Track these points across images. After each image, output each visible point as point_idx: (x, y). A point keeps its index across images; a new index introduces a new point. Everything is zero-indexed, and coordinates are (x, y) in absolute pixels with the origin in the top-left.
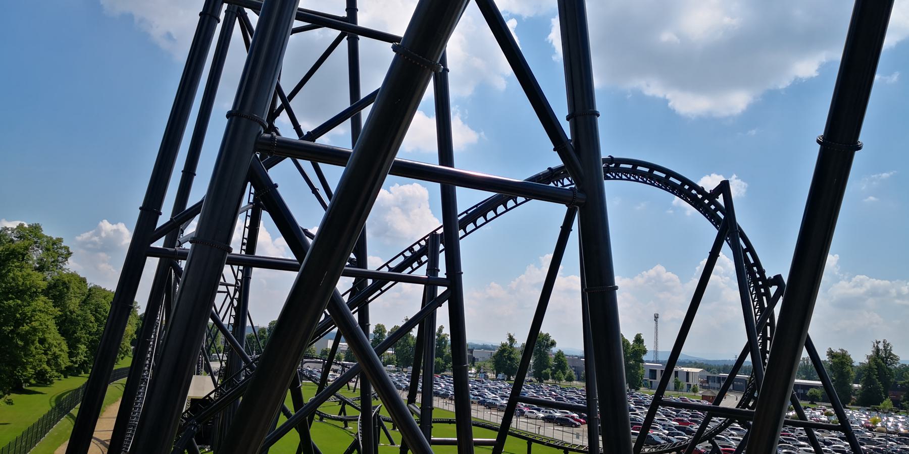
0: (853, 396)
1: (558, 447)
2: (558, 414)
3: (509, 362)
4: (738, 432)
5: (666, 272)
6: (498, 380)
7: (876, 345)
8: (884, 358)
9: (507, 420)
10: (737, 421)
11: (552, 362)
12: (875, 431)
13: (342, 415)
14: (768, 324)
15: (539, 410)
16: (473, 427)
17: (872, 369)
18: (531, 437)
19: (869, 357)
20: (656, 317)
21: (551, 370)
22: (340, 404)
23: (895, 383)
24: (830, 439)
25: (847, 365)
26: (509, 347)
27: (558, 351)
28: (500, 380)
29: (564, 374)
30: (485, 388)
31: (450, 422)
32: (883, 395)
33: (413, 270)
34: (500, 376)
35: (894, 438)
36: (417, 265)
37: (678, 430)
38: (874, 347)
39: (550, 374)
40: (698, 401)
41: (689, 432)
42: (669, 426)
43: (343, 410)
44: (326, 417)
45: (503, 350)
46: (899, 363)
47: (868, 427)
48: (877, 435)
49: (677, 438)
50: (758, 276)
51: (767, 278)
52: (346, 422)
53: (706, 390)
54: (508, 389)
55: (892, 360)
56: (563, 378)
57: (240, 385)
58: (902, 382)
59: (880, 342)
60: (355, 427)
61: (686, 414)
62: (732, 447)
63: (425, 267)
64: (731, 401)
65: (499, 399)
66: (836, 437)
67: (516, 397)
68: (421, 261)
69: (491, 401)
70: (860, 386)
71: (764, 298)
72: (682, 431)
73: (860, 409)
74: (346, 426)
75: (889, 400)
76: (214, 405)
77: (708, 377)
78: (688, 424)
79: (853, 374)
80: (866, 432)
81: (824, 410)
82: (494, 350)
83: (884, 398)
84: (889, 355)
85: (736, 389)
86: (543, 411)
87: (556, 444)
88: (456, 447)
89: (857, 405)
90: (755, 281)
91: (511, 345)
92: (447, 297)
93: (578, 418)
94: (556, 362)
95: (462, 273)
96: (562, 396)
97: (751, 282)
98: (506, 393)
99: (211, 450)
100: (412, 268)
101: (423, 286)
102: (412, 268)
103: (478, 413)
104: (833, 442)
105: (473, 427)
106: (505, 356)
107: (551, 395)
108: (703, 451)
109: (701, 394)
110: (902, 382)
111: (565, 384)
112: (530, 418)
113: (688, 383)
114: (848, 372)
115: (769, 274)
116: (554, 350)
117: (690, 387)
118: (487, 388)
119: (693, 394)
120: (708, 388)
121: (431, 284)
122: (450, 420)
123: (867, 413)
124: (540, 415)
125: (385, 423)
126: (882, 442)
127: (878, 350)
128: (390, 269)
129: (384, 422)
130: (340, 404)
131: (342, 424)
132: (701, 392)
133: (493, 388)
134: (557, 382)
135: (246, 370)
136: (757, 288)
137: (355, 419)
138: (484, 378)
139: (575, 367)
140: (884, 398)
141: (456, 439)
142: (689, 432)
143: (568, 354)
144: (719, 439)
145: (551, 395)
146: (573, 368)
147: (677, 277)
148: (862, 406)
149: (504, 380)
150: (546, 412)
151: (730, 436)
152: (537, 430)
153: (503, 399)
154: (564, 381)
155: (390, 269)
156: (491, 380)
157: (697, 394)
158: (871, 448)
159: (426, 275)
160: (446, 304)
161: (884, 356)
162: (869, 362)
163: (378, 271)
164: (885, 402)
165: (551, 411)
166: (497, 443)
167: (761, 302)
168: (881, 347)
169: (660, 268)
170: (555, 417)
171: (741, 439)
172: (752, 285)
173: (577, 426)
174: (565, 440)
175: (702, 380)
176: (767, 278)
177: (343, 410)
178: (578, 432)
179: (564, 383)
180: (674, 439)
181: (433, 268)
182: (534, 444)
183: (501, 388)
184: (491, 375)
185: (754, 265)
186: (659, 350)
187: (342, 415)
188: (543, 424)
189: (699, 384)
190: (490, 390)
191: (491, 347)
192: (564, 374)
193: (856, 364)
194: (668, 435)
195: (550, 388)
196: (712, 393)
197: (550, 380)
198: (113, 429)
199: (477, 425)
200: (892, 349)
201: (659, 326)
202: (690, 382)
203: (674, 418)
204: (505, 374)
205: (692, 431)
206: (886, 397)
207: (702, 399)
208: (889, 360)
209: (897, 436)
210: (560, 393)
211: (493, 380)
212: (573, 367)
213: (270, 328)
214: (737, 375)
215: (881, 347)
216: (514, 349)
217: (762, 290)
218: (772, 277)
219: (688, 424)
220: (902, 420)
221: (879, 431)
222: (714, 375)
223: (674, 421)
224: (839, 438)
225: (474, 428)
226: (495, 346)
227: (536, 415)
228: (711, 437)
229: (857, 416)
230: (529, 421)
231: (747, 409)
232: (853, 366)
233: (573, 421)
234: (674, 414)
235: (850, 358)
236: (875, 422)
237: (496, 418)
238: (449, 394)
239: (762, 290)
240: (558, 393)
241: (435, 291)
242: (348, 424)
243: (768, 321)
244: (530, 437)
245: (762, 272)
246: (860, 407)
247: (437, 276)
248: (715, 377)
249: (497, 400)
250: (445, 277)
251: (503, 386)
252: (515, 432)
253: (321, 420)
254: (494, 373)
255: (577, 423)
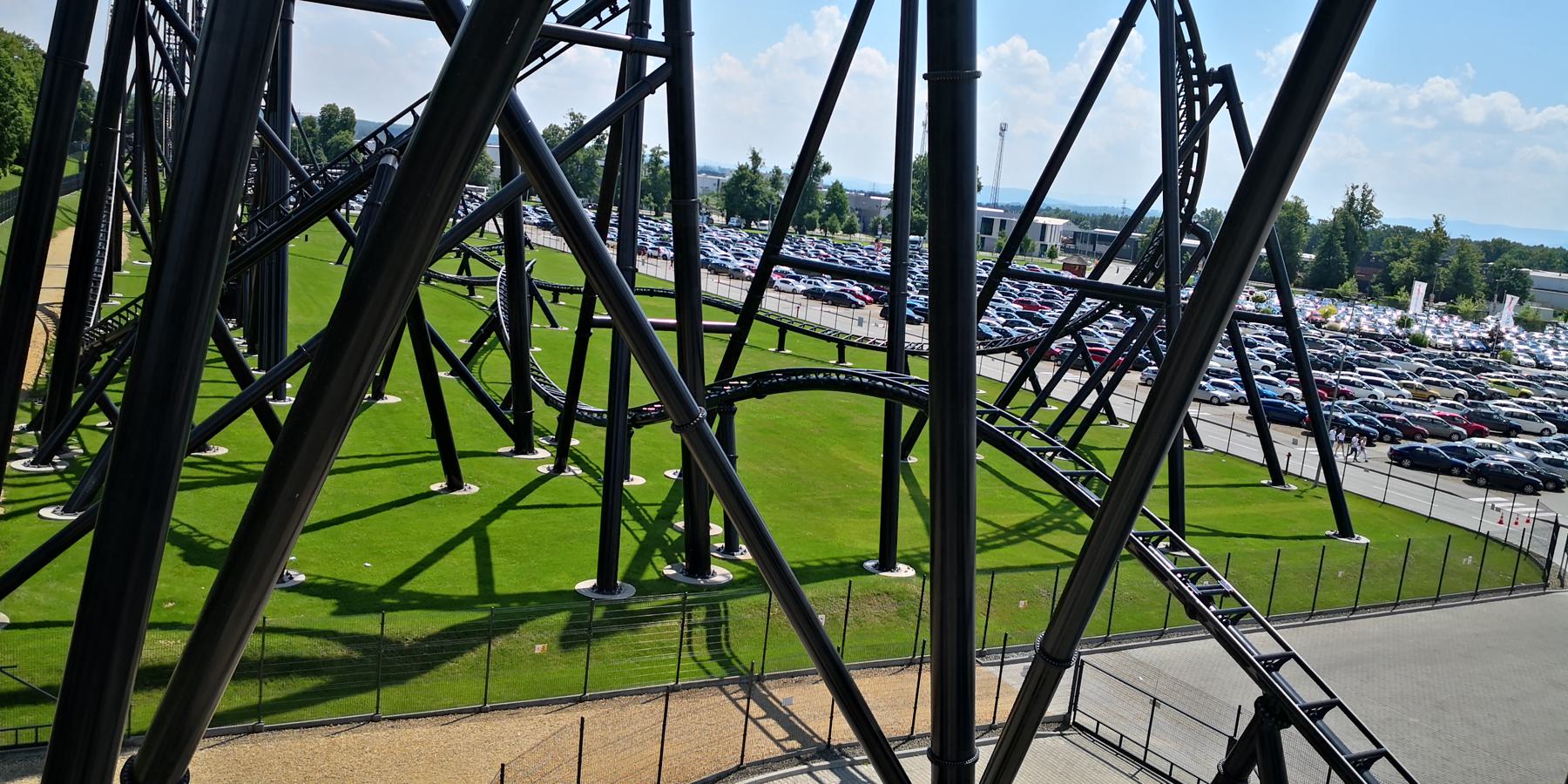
0: (1300, 272)
1: (829, 339)
2: (828, 286)
3: (749, 198)
4: (1115, 323)
5: (1028, 50)
6: (730, 227)
7: (1350, 193)
8: (1359, 213)
9: (755, 295)
10: (1121, 306)
11: (823, 201)
12: (1325, 328)
13: (464, 276)
14: (1196, 150)
15: (798, 279)
16: (703, 306)
17: (1337, 230)
18: (786, 322)
19: (1337, 212)
20: (1003, 130)
21: (820, 213)
22: (458, 256)
23: (1368, 254)
24: (1255, 338)
25: (1300, 222)
26: (750, 171)
27: (834, 181)
28: (733, 227)
29: (842, 221)
30: (708, 239)
31: (665, 294)
32: (1346, 273)
33: (602, 23)
34: (734, 221)
35: (1352, 340)
36: (610, 14)
37: (1021, 317)
38: (1347, 194)
39: (817, 221)
40: (1055, 272)
41: (1039, 322)
42: (1008, 310)
43: (464, 267)
44: (435, 277)
45: (740, 176)
46: (1380, 222)
47: (1314, 322)
48: (1327, 335)
49: (1018, 331)
50: (1193, 65)
51: (1208, 70)
52: (472, 285)
53: (1070, 255)
54: (747, 243)
55: (1371, 217)
56: (839, 228)
57: (293, 217)
58: (1379, 253)
59: (1357, 187)
60: (494, 296)
61: (1035, 292)
62: (1103, 346)
63: (624, 18)
64: (1117, 274)
65: (732, 258)
66: (1265, 335)
67: (772, 256)
68: (617, 7)
69: (718, 261)
70: (1313, 256)
71: (1197, 104)
72: (1026, 319)
73: (1307, 293)
74: (472, 293)
75: (1355, 280)
76: (248, 249)
77: (1075, 233)
78: (1037, 308)
79: (1306, 238)
80: (1311, 329)
81: (1251, 293)
82: (723, 175)
83: (1346, 277)
84: (1368, 210)
85: (1125, 258)
86: (805, 281)
87: (826, 334)
88: (675, 333)
89: (1303, 287)
90: (1187, 73)
91: (755, 168)
92: (665, 79)
93: (861, 294)
94: (829, 201)
95: (693, 34)
96: (836, 257)
97: (1180, 75)
98: (745, 249)
99: (239, 326)
100: (600, 19)
101: (620, 54)
102: (600, 19)
103: (710, 284)
104: (1258, 342)
105: (703, 306)
106: (743, 187)
107: (818, 255)
108: (1058, 350)
109: (1061, 261)
110: (1379, 253)
111: (841, 238)
112: (784, 291)
113: (1042, 243)
114: (1299, 234)
115: (1212, 64)
116: (827, 180)
117: (1045, 250)
118: (712, 240)
119: (1049, 261)
120: (1074, 252)
121: (636, 51)
122: (652, 289)
123: (1317, 300)
124: (799, 286)
125: (542, 292)
126: (1333, 346)
127: (1352, 199)
128: (560, 20)
129: (539, 290)
130: (458, 256)
131: (464, 290)
132: (1061, 259)
133: (722, 240)
134: (829, 234)
135: (301, 192)
136: (1188, 86)
137: (490, 282)
138: (707, 224)
139: (860, 210)
140: (1346, 277)
141: (675, 321)
142: (1039, 322)
143: (848, 189)
144: (1085, 333)
145: (818, 255)
146: (857, 212)
147: (1046, 59)
148: (1309, 288)
149: (740, 227)
150: (810, 283)
151: (1101, 328)
152: (795, 311)
153: (738, 259)
154: (841, 232)
155: (560, 20)
156: (719, 226)
157: (1055, 261)
158: (1315, 354)
159: (627, 34)
160: (662, 90)
161: (1359, 209)
162: (1334, 219)
163: (594, 31)
164: (1347, 284)
165: (819, 281)
166: (738, 329)
167: (1190, 111)
168: (1358, 195)
169: (1018, 42)
170: (824, 290)
171: (1121, 334)
172: (1181, 81)
173: (859, 307)
174: (840, 328)
175: (1065, 238)
176: (1208, 70)
177: (464, 267)
178: (862, 316)
179: (840, 236)
180: (1014, 332)
181: (639, 23)
182: (789, 333)
183: (735, 241)
184: (718, 219)
185: (1190, 45)
186: (1001, 186)
187: (464, 276)
188: (804, 302)
189: (1059, 244)
190: (716, 243)
191: (717, 170)
192: (842, 221)
193: (1313, 221)
194: (1003, 325)
195: (816, 244)
196: (1080, 259)
197: (817, 231)
198: (42, 291)
199: (709, 302)
200: (1375, 198)
201: (1005, 145)
202: (1047, 241)
203: (1015, 298)
204: (742, 217)
205: (1043, 319)
206: (1350, 276)
207: (1063, 269)
208: (1366, 216)
209: (1357, 336)
210: (832, 253)
211: (721, 227)
212: (856, 210)
213: (322, 116)
214: (1133, 234)
215: (1358, 195)
216: (760, 175)
217: (1196, 91)
218: (1216, 69)
219: (1037, 308)
220: (1367, 313)
221: (1332, 329)
222: (1087, 231)
223: (1015, 302)
224: (1269, 336)
225: (704, 307)
226: (724, 169)
227: (793, 287)
228: (1075, 330)
229: (1305, 304)
230: (783, 296)
231: (1140, 287)
232: (1308, 224)
233: (852, 298)
234: (1016, 293)
235: (1306, 211)
236: (1326, 315)
237: (737, 293)
238: (648, 247)
239: (1196, 91)
240: (829, 253)
241: (641, 65)
242: (476, 290)
243: (1197, 144)
244: (783, 321)
245: (1200, 58)
246: (1307, 291)
247: (647, 37)
248: (1087, 234)
249: (730, 261)
250: (662, 39)
251: (739, 238)
252: (771, 317)
253: (427, 281)
254: (723, 216)
255: (860, 302)
